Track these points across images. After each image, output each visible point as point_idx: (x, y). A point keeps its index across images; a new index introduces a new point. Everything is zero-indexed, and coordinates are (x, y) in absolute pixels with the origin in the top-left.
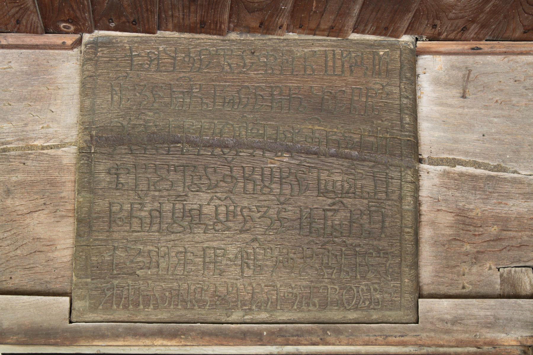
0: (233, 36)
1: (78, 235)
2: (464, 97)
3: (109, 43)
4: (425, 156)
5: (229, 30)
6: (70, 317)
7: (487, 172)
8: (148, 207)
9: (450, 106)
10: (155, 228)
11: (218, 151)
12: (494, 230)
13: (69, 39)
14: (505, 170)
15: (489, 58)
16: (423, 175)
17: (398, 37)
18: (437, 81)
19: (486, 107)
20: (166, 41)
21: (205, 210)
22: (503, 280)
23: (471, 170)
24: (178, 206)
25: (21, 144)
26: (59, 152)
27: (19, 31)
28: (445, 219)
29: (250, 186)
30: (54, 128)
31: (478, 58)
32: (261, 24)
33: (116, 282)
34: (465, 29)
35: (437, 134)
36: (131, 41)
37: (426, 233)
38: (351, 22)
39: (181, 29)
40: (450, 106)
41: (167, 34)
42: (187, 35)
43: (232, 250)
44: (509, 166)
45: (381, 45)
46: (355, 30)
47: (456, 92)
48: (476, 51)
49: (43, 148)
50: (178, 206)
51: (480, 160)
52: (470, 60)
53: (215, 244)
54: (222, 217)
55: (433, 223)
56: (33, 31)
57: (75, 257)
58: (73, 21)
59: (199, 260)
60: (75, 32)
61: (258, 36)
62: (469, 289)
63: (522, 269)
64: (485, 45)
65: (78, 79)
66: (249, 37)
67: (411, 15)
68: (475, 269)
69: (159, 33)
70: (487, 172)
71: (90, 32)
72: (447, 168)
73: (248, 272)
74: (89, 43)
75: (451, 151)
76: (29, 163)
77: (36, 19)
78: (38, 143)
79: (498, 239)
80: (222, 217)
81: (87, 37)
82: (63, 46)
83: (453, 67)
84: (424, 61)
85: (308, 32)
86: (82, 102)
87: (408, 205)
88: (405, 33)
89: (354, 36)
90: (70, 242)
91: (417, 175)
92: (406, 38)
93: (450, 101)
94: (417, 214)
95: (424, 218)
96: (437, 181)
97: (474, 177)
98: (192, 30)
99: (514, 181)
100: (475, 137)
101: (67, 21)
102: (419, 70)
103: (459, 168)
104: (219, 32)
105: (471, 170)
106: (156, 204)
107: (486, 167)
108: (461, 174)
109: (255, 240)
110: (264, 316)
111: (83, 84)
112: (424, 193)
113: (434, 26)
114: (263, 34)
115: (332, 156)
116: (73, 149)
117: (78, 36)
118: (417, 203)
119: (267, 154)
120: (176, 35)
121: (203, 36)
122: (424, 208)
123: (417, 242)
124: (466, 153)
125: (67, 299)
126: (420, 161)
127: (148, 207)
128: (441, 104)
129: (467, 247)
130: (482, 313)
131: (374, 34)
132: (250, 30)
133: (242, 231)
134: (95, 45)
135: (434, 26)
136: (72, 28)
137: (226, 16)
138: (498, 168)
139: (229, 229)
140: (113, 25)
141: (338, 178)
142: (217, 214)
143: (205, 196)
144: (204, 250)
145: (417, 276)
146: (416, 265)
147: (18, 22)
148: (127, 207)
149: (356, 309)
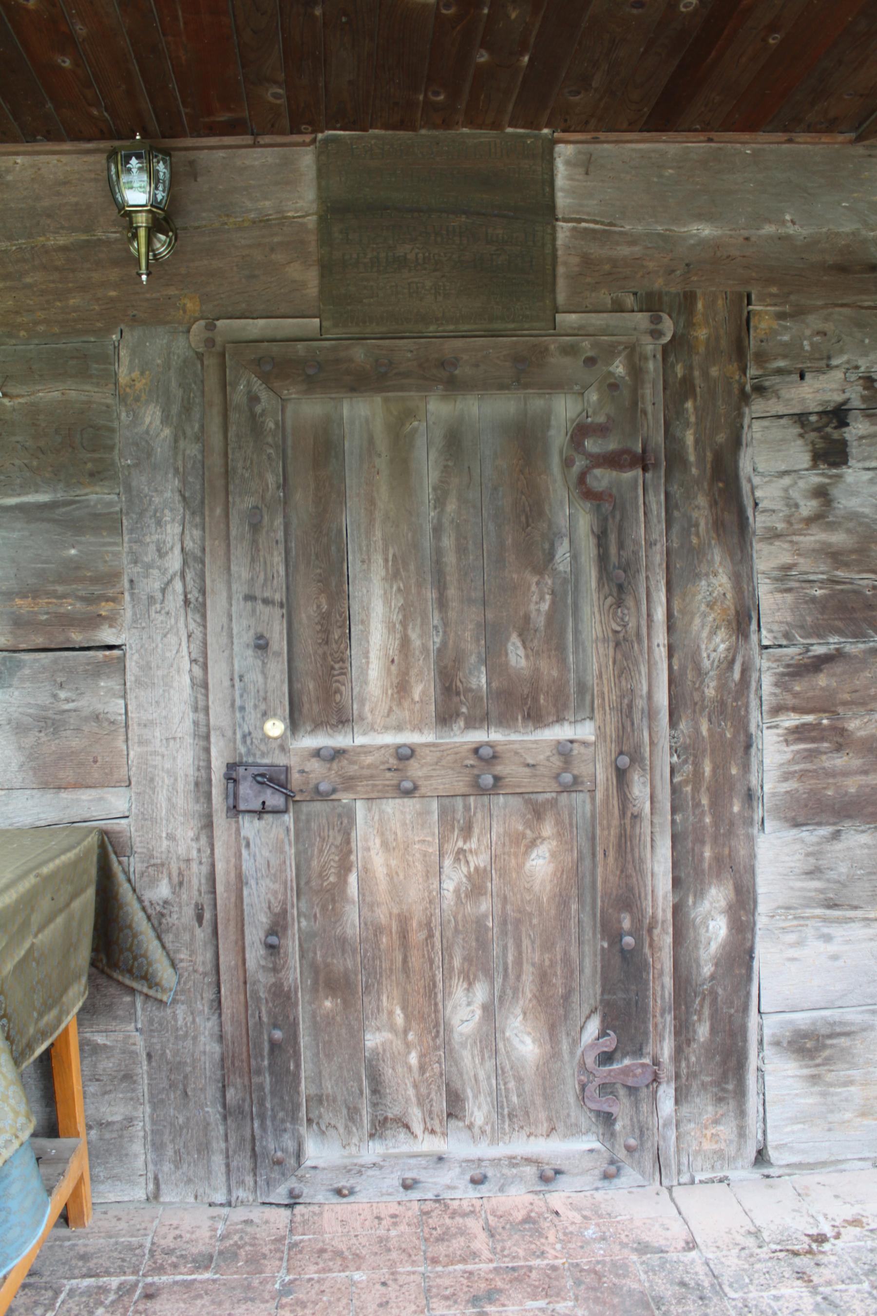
0: (423, 132)
1: (322, 276)
2: (587, 173)
3: (335, 140)
4: (560, 216)
5: (422, 127)
6: (205, 634)
7: (602, 227)
8: (369, 256)
9: (578, 180)
10: (375, 269)
11: (416, 214)
12: (607, 267)
13: (308, 138)
14: (615, 225)
15: (606, 146)
16: (559, 230)
17: (540, 129)
18: (568, 163)
19: (603, 181)
20: (376, 137)
21: (409, 257)
22: (614, 301)
23: (592, 226)
24: (390, 254)
25: (279, 216)
26: (306, 220)
27: (272, 133)
28: (575, 260)
29: (439, 239)
30: (301, 203)
31: (598, 146)
32: (444, 121)
33: (349, 308)
34: (587, 123)
35: (568, 201)
36: (351, 138)
37: (561, 270)
38: (507, 118)
39: (386, 127)
40: (578, 180)
41: (376, 131)
42: (390, 132)
43: (428, 284)
44: (618, 222)
45: (527, 136)
46: (510, 126)
47: (582, 170)
48: (596, 141)
49: (294, 217)
50: (390, 254)
51: (598, 219)
52: (591, 147)
53: (416, 280)
54: (420, 261)
55: (565, 263)
56: (282, 133)
57: (321, 292)
58: (311, 123)
59: (406, 291)
60: (312, 133)
61: (442, 132)
62: (590, 307)
63: (562, 190)
64: (602, 136)
65: (314, 167)
66: (435, 133)
67: (548, 111)
68: (593, 295)
69: (371, 131)
70: (602, 227)
71: (322, 132)
72: (574, 224)
73: (440, 298)
74: (322, 140)
75: (578, 213)
76: (285, 228)
77: (286, 122)
78: (289, 214)
79: (610, 274)
80: (420, 261)
81: (320, 136)
82: (304, 144)
83: (579, 152)
84: (560, 148)
85: (691, 1033)
86: (319, 184)
87: (548, 250)
88: (546, 127)
89: (510, 130)
90: (316, 282)
91: (554, 228)
92: (546, 131)
93: (577, 177)
94: (555, 257)
95: (560, 260)
96: (568, 234)
97: (594, 231)
98: (394, 128)
99: (621, 233)
100: (595, 202)
101: (307, 124)
102: (556, 155)
103: (584, 225)
104: (414, 129)
105: (592, 226)
106: (375, 254)
107: (602, 223)
108: (585, 229)
109: (443, 276)
110: (451, 327)
111: (319, 170)
112: (559, 242)
113: (566, 121)
114: (445, 129)
115: (495, 216)
116: (315, 218)
117: (313, 136)
118: (554, 250)
119: (451, 216)
120: (383, 132)
121: (402, 133)
122: (560, 253)
123: (554, 276)
124: (588, 214)
125: (318, 320)
126: (557, 220)
127: (369, 256)
128: (572, 179)
129: (588, 280)
130: (599, 322)
131: (523, 127)
132: (435, 127)
133: (435, 270)
134: (327, 141)
135: (566, 121)
136: (310, 129)
137: (419, 115)
138: (611, 224)
139: (425, 269)
140: (338, 125)
141: (500, 232)
142: (417, 259)
143: (408, 247)
144: (409, 284)
145: (554, 299)
146: (553, 291)
147: (273, 126)
148: (355, 256)
149: (513, 321)
